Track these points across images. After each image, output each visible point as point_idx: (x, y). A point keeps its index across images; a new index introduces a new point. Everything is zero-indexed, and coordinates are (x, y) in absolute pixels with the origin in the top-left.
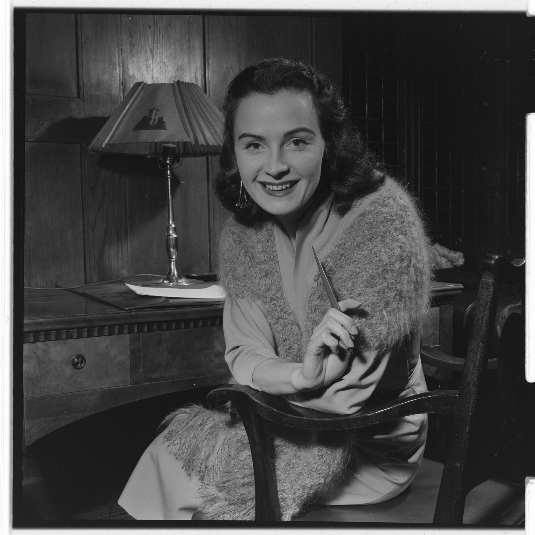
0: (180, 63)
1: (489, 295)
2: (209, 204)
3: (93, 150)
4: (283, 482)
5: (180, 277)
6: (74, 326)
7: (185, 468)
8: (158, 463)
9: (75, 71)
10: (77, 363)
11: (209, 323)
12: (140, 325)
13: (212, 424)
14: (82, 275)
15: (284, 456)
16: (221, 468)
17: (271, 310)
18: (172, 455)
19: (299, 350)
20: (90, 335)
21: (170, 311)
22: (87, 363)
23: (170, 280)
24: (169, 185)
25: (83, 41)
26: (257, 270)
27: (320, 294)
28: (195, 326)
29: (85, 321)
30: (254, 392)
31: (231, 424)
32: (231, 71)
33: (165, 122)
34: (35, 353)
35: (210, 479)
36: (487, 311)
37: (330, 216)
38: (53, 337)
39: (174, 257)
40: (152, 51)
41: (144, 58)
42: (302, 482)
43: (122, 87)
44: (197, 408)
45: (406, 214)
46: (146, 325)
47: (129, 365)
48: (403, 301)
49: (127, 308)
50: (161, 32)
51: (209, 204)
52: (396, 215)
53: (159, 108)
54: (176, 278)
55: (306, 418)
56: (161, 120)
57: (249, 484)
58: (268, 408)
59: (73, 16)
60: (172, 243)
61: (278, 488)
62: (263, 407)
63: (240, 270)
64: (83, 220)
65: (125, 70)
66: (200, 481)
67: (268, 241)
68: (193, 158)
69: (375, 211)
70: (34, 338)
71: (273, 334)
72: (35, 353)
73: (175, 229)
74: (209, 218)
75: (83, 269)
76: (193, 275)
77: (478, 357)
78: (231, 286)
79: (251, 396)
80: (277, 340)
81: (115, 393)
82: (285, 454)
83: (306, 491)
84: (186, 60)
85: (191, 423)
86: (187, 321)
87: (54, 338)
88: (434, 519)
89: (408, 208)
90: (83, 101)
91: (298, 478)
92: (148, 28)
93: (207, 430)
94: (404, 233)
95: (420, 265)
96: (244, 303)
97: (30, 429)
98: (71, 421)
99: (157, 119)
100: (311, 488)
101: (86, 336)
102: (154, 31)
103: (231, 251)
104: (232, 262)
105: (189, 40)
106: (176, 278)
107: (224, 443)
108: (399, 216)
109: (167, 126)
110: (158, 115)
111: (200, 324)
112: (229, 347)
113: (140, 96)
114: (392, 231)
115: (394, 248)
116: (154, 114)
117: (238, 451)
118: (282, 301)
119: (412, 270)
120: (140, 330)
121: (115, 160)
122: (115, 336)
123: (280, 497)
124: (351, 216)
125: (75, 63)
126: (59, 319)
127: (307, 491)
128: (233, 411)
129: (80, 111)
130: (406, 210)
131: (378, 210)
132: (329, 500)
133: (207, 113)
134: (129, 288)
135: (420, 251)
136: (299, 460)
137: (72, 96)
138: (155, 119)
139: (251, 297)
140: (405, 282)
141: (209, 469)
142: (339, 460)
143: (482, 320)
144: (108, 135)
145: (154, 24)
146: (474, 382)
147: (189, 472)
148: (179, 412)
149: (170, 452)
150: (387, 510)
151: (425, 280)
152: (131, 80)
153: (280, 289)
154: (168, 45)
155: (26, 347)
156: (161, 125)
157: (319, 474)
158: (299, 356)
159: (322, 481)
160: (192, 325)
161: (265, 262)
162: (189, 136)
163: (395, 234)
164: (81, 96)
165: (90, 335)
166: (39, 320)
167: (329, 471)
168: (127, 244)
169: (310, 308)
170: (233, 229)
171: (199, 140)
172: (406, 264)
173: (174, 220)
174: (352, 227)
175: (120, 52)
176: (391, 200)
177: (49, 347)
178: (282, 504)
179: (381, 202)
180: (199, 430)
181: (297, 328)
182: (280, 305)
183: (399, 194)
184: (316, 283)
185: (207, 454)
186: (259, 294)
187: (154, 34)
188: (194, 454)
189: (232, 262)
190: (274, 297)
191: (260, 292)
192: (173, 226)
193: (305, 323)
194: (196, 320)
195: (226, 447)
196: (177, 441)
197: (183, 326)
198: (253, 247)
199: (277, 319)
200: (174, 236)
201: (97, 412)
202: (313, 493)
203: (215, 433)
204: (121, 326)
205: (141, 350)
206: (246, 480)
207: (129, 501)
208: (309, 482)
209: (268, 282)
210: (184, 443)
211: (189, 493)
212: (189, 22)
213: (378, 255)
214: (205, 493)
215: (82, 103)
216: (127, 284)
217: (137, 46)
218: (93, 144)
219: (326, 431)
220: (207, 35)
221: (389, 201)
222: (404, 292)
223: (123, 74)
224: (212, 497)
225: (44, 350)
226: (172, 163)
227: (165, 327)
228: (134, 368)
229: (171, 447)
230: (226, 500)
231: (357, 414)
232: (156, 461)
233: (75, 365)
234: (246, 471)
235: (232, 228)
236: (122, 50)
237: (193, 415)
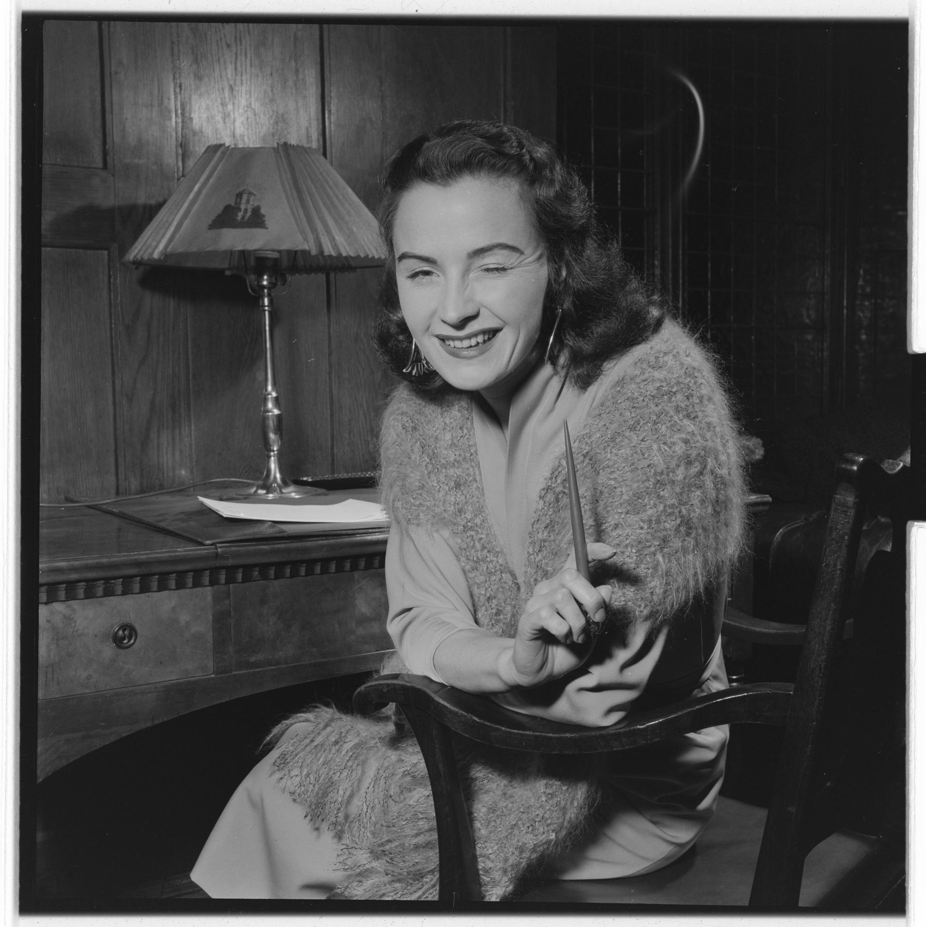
0: (281, 111)
1: (848, 523)
3: (137, 263)
4: (486, 842)
5: (285, 483)
6: (117, 573)
7: (309, 817)
8: (263, 808)
9: (99, 123)
10: (124, 636)
11: (348, 565)
12: (231, 570)
13: (356, 741)
14: (112, 479)
15: (485, 795)
16: (373, 819)
17: (465, 546)
18: (287, 795)
19: (513, 616)
20: (145, 589)
21: (282, 546)
23: (269, 489)
24: (267, 323)
25: (113, 69)
26: (442, 479)
27: (548, 521)
28: (325, 571)
29: (137, 564)
30: (436, 688)
31: (395, 742)
32: (368, 125)
33: (263, 216)
35: (353, 836)
36: (844, 551)
37: (565, 387)
38: (81, 593)
39: (275, 449)
40: (232, 89)
41: (219, 101)
42: (518, 841)
43: (180, 151)
44: (327, 712)
45: (695, 383)
46: (241, 570)
47: (211, 640)
48: (693, 535)
49: (208, 542)
50: (249, 56)
52: (678, 383)
53: (252, 191)
54: (278, 485)
55: (531, 733)
56: (256, 211)
57: (427, 845)
58: (465, 716)
59: (95, 24)
60: (271, 424)
61: (478, 853)
62: (456, 714)
63: (414, 478)
64: (114, 382)
65: (186, 119)
66: (336, 840)
67: (461, 428)
68: (305, 275)
69: (642, 377)
70: (48, 596)
71: (469, 588)
73: (277, 401)
75: (113, 469)
76: (305, 479)
77: (828, 628)
78: (399, 504)
79: (433, 695)
80: (476, 599)
81: (186, 690)
82: (487, 792)
83: (524, 855)
84: (292, 106)
85: (319, 740)
86: (311, 563)
87: (82, 595)
88: (750, 902)
89: (699, 371)
91: (511, 833)
92: (225, 47)
93: (347, 752)
94: (693, 415)
95: (724, 472)
96: (419, 534)
98: (113, 739)
99: (250, 210)
100: (534, 850)
101: (138, 591)
102: (236, 54)
103: (400, 445)
104: (401, 464)
105: (297, 71)
106: (278, 485)
107: (383, 774)
108: (682, 386)
109: (268, 222)
110: (251, 203)
111: (333, 567)
112: (394, 609)
113: (219, 168)
114: (672, 413)
115: (674, 443)
116: (244, 201)
117: (404, 790)
118: (485, 532)
119: (708, 481)
120: (230, 580)
121: (171, 278)
122: (188, 591)
123: (480, 867)
124: (600, 388)
125: (98, 108)
126: (90, 561)
127: (526, 855)
128: (400, 720)
129: (108, 195)
130: (696, 374)
131: (647, 375)
132: (564, 871)
133: (335, 200)
134: (202, 504)
135: (724, 445)
136: (512, 803)
137: (93, 166)
138: (246, 210)
139: (432, 524)
140: (696, 502)
141: (351, 819)
142: (581, 801)
143: (835, 566)
144: (163, 236)
145: (236, 40)
146: (820, 669)
147: (317, 825)
148: (296, 720)
149: (284, 790)
150: (656, 887)
151: (731, 495)
152: (196, 138)
153: (480, 510)
154: (260, 79)
156: (257, 220)
157: (548, 826)
158: (512, 626)
159: (553, 836)
160: (318, 569)
161: (456, 463)
162: (306, 240)
163: (676, 418)
166: (58, 564)
167: (564, 819)
168: (190, 426)
169: (533, 543)
170: (404, 407)
171: (324, 246)
172: (696, 470)
173: (275, 384)
174: (602, 404)
175: (178, 90)
176: (671, 356)
177: (74, 610)
178: (485, 879)
179: (652, 359)
180: (334, 751)
181: (510, 578)
182: (481, 539)
183: (684, 347)
184: (542, 502)
185: (348, 793)
186: (444, 518)
187: (236, 59)
188: (325, 794)
189: (401, 464)
190: (469, 524)
191: (446, 515)
192: (274, 394)
193: (524, 569)
194: (325, 562)
195: (382, 781)
196: (296, 772)
197: (303, 570)
198: (436, 438)
199: (476, 562)
200: (276, 412)
201: (157, 722)
202: (537, 858)
203: (361, 758)
204: (198, 573)
205: (232, 614)
206: (421, 840)
207: (207, 875)
208: (530, 840)
209: (460, 498)
210: (308, 775)
211: (317, 860)
212: (296, 39)
213: (646, 455)
214: (349, 862)
215: (112, 178)
216: (201, 499)
217: (206, 79)
218: (136, 251)
219: (562, 754)
220: (327, 61)
221: (666, 358)
222: (695, 520)
223: (182, 128)
224: (361, 868)
225: (64, 616)
226: (272, 286)
227: (272, 572)
228: (220, 644)
229: (284, 781)
230: (387, 874)
231: (618, 727)
232: (258, 807)
233: (118, 641)
234: (421, 823)
235: (402, 405)
236: (180, 86)
237: (321, 726)
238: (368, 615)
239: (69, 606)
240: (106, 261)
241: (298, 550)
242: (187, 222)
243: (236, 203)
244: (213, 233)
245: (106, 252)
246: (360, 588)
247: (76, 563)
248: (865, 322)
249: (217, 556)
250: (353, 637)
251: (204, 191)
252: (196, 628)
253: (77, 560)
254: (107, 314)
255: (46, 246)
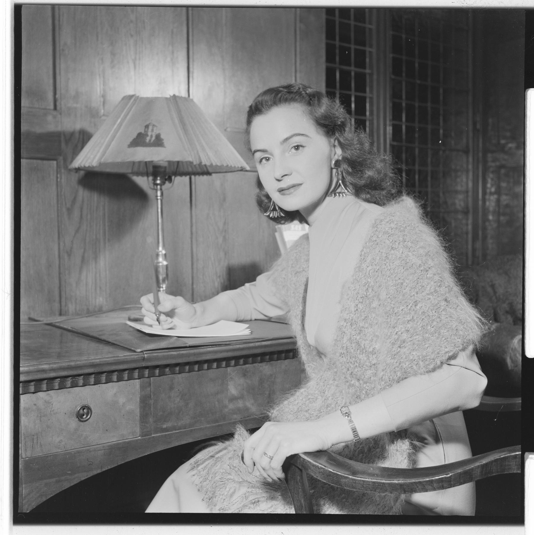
2: (192, 226)
3: (78, 170)
10: (83, 413)
22: (93, 414)
29: (93, 365)
33: (163, 140)
34: (35, 405)
39: (164, 286)
47: (139, 415)
51: (192, 226)
53: (155, 124)
56: (158, 137)
58: (323, 469)
72: (35, 405)
74: (192, 241)
90: (61, 114)
97: (29, 494)
105: (173, 52)
109: (165, 142)
110: (155, 131)
121: (96, 180)
138: (152, 136)
144: (98, 151)
155: (24, 399)
156: (158, 142)
164: (58, 108)
165: (97, 382)
173: (164, 246)
192: (164, 252)
200: (165, 263)
201: (104, 470)
205: (152, 396)
212: (172, 32)
215: (59, 116)
225: (45, 401)
228: (144, 417)
233: (80, 416)
238: (236, 395)
239: (49, 394)
240: (55, 168)
241: (195, 354)
242: (113, 143)
243: (145, 131)
244: (132, 150)
245: (55, 162)
246: (231, 378)
247: (55, 366)
248: (491, 209)
249: (144, 359)
250: (226, 410)
251: (124, 124)
252: (129, 407)
253: (55, 363)
254: (55, 201)
255: (23, 158)
